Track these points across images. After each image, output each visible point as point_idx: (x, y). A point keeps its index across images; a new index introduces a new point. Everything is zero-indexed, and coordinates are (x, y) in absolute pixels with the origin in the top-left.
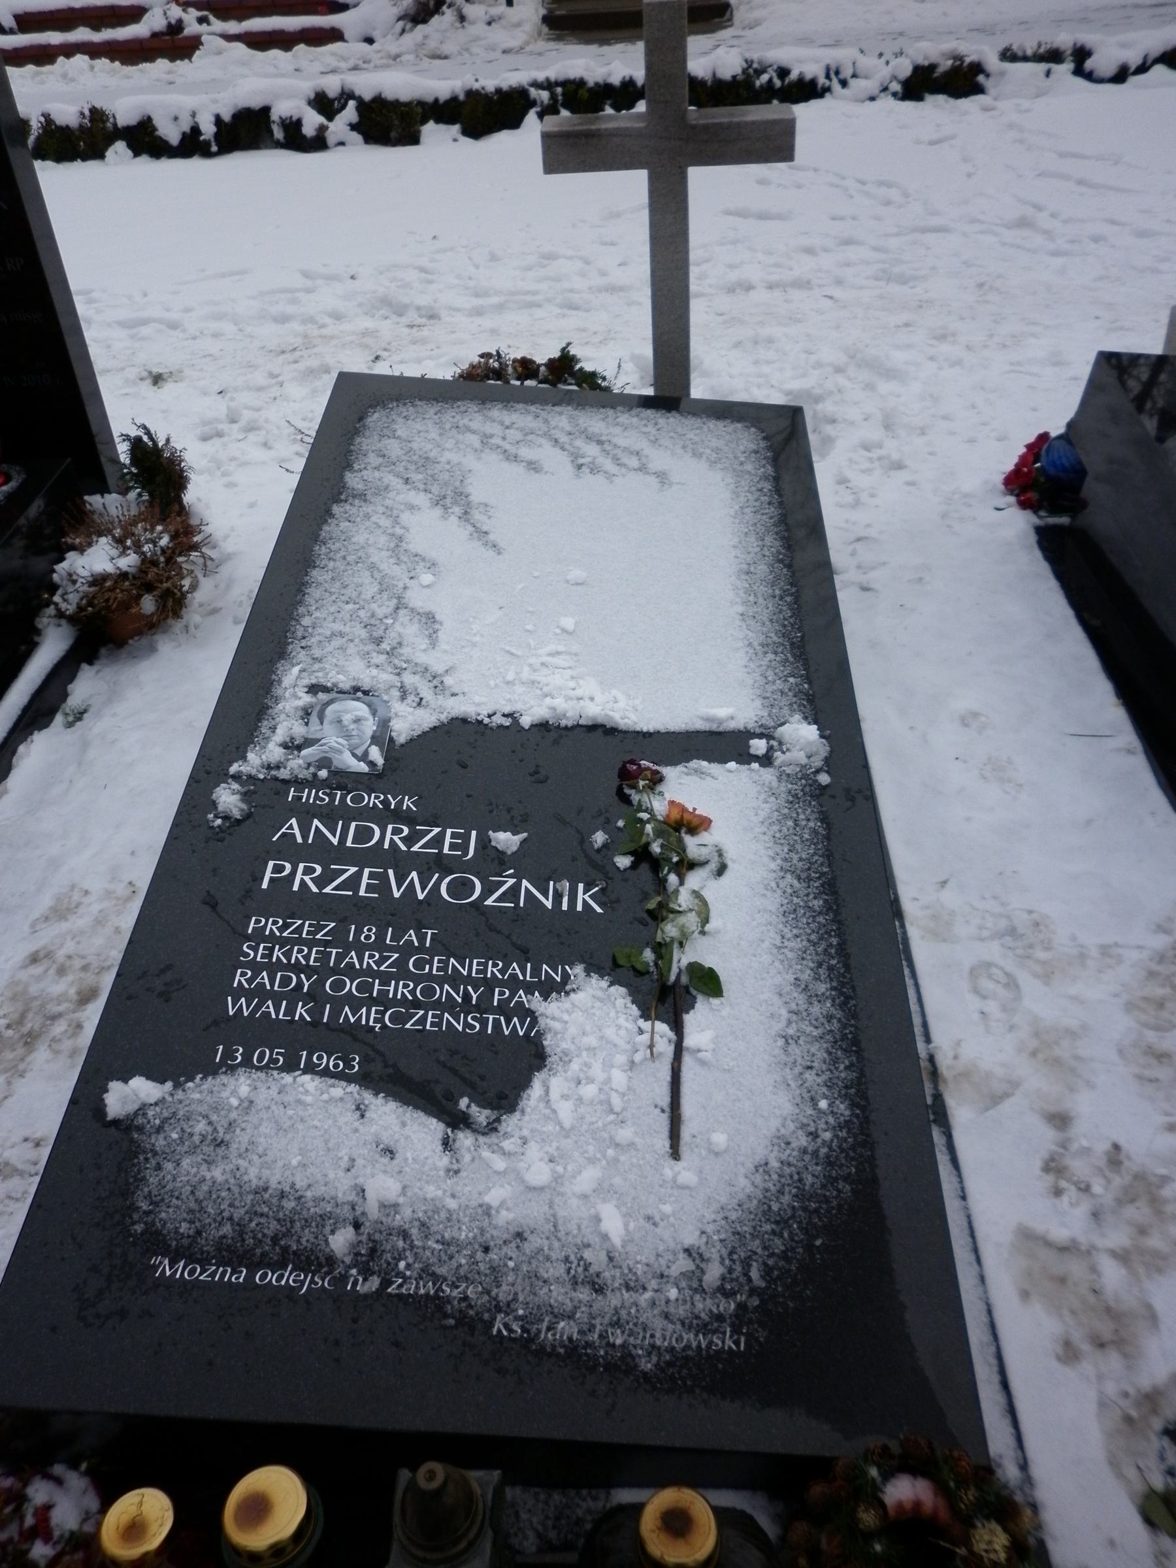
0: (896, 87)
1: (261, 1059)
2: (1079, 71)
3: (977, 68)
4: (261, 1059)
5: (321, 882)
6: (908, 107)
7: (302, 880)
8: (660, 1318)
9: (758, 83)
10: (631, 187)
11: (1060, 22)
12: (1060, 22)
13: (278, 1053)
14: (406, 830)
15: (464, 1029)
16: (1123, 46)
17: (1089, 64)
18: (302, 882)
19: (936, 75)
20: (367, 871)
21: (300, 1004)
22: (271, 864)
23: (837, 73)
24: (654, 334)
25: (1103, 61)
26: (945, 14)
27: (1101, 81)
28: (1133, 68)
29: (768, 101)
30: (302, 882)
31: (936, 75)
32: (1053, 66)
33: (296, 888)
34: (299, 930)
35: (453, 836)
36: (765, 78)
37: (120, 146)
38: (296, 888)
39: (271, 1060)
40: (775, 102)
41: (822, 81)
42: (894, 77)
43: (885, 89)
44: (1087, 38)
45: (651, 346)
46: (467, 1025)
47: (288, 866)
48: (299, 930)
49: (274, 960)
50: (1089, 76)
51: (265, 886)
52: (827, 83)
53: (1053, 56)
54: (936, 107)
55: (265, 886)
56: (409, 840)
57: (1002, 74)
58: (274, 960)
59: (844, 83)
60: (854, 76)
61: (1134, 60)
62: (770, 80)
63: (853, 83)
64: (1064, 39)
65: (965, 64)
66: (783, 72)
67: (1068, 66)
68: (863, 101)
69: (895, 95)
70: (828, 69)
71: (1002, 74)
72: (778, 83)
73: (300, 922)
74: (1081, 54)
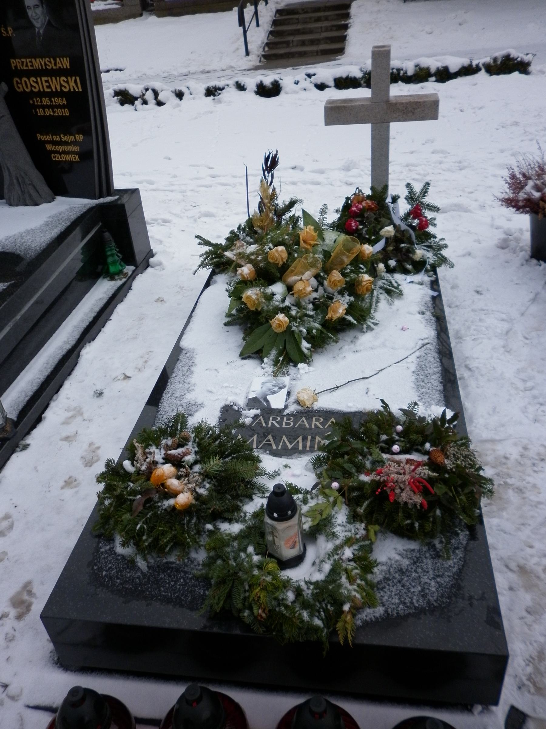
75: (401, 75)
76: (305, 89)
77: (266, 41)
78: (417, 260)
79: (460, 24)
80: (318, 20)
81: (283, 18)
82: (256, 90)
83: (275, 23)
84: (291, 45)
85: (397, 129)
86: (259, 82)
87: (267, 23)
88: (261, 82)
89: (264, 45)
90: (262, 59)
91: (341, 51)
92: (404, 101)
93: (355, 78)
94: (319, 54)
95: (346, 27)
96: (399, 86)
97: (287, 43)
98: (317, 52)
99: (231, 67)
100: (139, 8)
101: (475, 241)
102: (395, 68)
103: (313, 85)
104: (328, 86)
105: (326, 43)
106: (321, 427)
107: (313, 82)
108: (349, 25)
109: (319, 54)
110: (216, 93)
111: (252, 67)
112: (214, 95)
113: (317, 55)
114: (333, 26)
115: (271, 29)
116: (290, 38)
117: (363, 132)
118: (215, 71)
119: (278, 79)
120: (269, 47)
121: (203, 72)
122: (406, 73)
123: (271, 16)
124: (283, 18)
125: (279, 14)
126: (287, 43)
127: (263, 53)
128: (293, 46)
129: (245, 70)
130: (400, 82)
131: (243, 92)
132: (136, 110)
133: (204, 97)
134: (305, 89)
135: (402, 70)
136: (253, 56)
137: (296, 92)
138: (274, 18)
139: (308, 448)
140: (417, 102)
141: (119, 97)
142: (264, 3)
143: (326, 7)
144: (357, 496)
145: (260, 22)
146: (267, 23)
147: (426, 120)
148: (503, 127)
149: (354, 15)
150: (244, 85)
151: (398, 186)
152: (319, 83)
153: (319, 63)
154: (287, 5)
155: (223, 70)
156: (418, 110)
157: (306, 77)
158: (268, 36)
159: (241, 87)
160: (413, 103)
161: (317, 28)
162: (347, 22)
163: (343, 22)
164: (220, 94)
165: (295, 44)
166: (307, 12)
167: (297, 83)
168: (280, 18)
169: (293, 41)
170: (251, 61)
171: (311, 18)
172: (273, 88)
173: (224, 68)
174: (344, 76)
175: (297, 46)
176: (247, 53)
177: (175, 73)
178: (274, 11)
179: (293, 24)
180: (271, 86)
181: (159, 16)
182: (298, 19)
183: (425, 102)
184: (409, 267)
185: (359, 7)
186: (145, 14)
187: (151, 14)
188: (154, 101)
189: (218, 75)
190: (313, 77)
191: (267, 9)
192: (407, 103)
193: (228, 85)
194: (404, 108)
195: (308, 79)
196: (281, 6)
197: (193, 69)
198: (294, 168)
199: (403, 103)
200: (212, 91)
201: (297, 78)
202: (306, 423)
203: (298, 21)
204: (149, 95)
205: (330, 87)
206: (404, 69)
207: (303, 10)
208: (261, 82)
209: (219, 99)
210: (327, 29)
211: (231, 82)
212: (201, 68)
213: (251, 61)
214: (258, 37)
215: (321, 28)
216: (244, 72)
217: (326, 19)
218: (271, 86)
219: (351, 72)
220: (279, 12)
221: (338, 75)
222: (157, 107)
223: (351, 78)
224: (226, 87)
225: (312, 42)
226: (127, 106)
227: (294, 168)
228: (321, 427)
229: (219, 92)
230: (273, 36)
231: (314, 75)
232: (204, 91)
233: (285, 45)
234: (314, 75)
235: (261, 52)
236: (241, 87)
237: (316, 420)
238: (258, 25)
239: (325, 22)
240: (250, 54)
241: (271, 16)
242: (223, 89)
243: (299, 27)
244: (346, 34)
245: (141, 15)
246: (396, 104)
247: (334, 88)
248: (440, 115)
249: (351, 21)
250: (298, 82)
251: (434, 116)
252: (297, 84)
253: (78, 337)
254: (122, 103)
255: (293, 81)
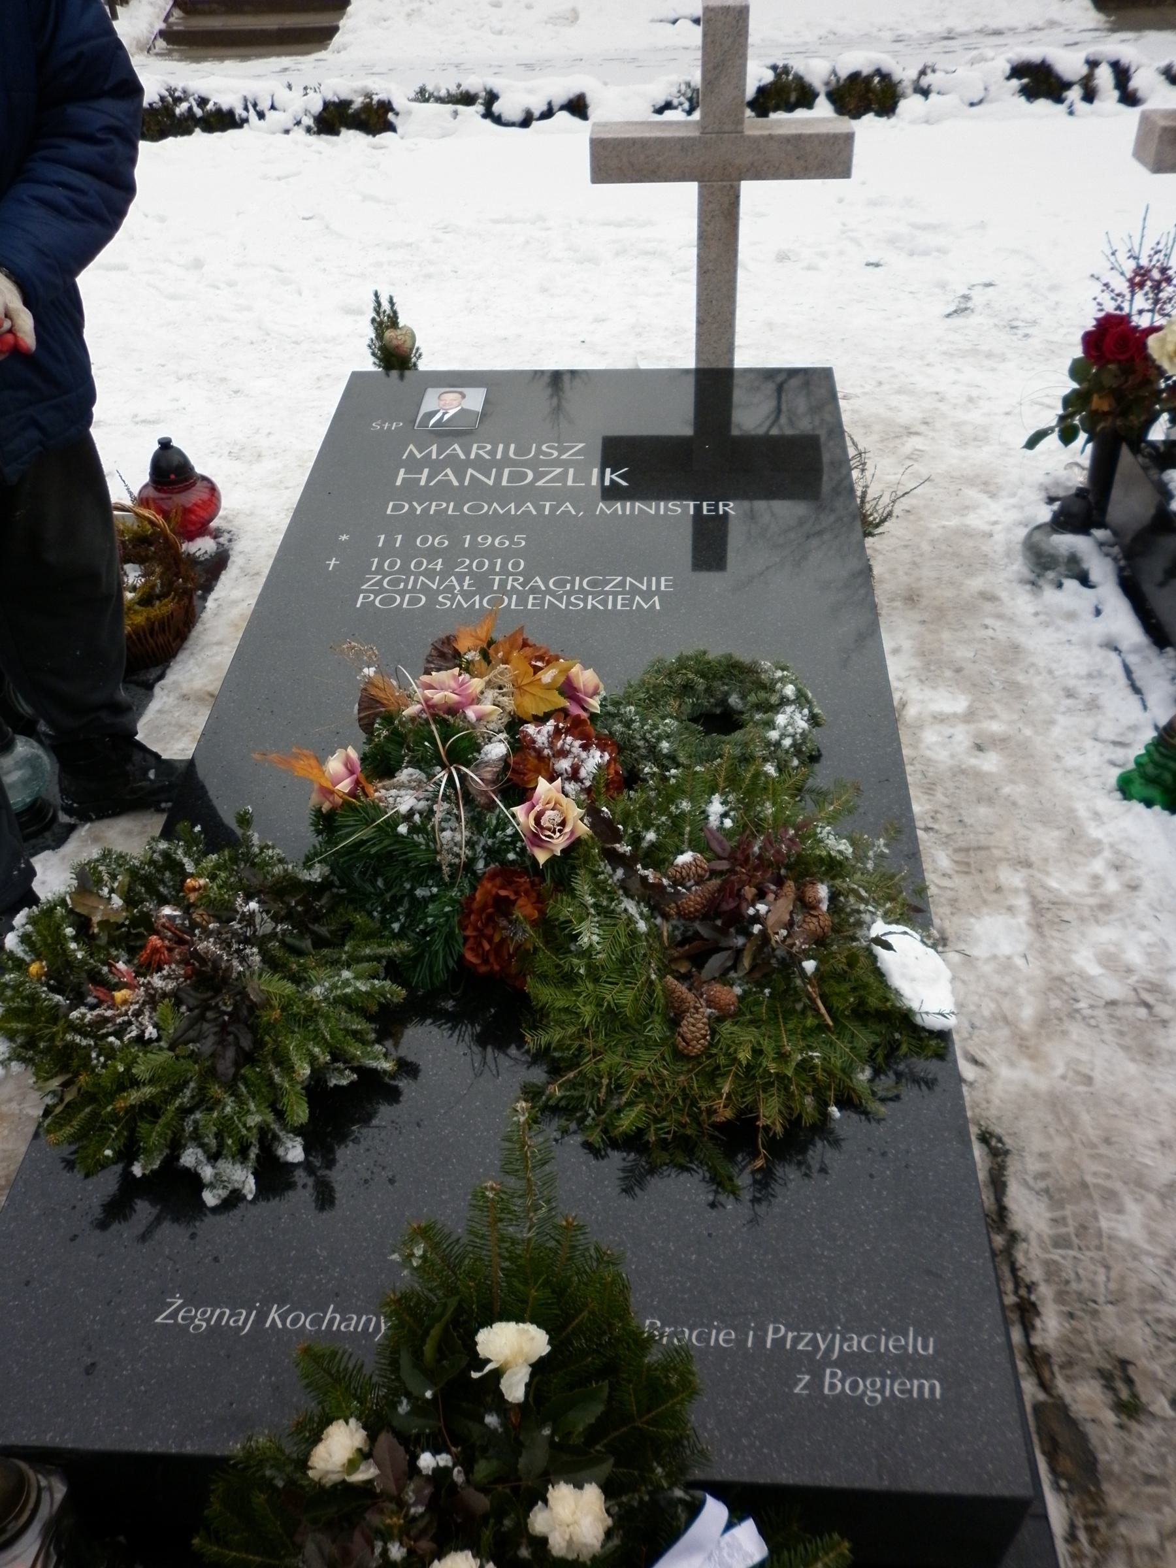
0: (308, 121)
2: (488, 114)
3: (386, 107)
6: (324, 142)
8: (553, 1556)
9: (178, 111)
11: (867, 39)
12: (867, 39)
16: (530, 91)
17: (497, 108)
19: (351, 111)
23: (255, 105)
24: (735, 271)
25: (505, 107)
26: (516, 47)
27: (512, 124)
28: (537, 114)
29: (188, 132)
31: (351, 111)
32: (460, 108)
36: (184, 106)
40: (198, 130)
41: (239, 111)
42: (306, 112)
43: (298, 123)
44: (496, 84)
45: (695, 288)
50: (498, 120)
52: (244, 114)
53: (467, 99)
54: (351, 139)
57: (409, 113)
59: (261, 115)
60: (273, 107)
61: (538, 108)
62: (190, 108)
63: (270, 115)
64: (473, 83)
65: (374, 102)
66: (203, 102)
67: (479, 108)
68: (274, 133)
69: (309, 130)
70: (245, 100)
71: (409, 113)
72: (198, 112)
74: (492, 97)
85: (754, 195)
117: (676, 204)
132: (1071, 113)
139: (611, 597)
141: (1025, 81)
144: (147, 668)
173: (1040, 24)
188: (1116, 94)
202: (540, 583)
204: (1104, 77)
212: (978, 23)
222: (1122, 108)
226: (1043, 105)
237: (514, 580)
248: (855, 170)
251: (844, 172)
254: (1030, 93)
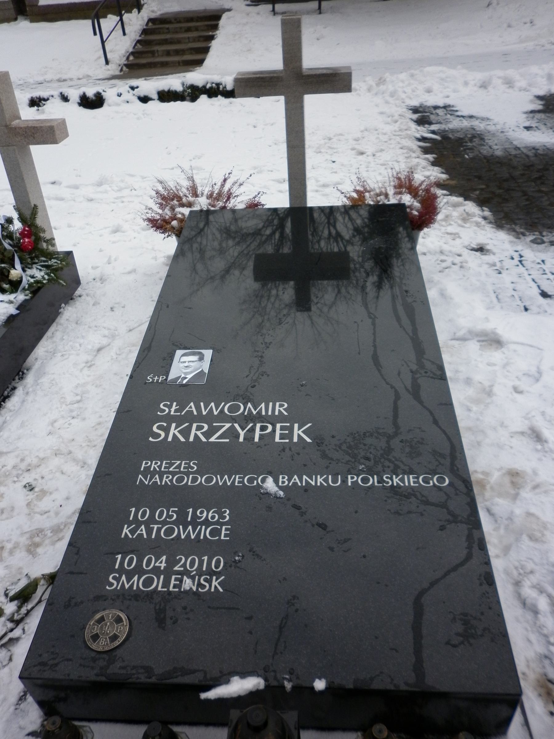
1: (160, 516)
4: (160, 516)
5: (208, 435)
7: (196, 434)
10: (314, 200)
13: (173, 511)
14: (206, 427)
15: (197, 589)
18: (196, 435)
20: (183, 462)
21: (126, 526)
22: (144, 462)
30: (196, 435)
33: (152, 469)
34: (179, 466)
35: (282, 428)
37: (159, 65)
38: (152, 469)
39: (169, 516)
46: (200, 585)
47: (150, 462)
48: (179, 466)
49: (295, 439)
51: (142, 469)
55: (142, 469)
56: (208, 435)
58: (295, 439)
73: (179, 462)
75: (221, 89)
76: (128, 102)
77: (131, 50)
78: (14, 280)
79: (318, 39)
80: (188, 30)
81: (157, 26)
82: (79, 101)
83: (145, 32)
84: (156, 55)
86: (82, 93)
87: (135, 32)
88: (84, 94)
89: (128, 54)
90: (124, 68)
91: (200, 63)
92: (22, 126)
93: (176, 92)
94: (181, 64)
95: (212, 38)
96: (219, 100)
97: (153, 53)
98: (179, 62)
99: (88, 76)
100: (12, 12)
101: (153, 258)
102: (215, 82)
103: (136, 98)
104: (151, 99)
105: (191, 54)
106: (204, 440)
107: (136, 94)
108: (215, 36)
109: (181, 64)
110: (41, 104)
111: (108, 77)
112: (38, 106)
113: (179, 65)
114: (200, 37)
115: (140, 38)
116: (156, 48)
118: (71, 79)
119: (101, 91)
120: (134, 56)
121: (59, 80)
122: (225, 87)
123: (141, 25)
124: (157, 26)
125: (152, 23)
126: (153, 53)
127: (126, 62)
128: (158, 56)
129: (99, 79)
130: (219, 96)
131: (67, 103)
133: (28, 107)
134: (128, 102)
135: (222, 84)
136: (113, 65)
137: (118, 105)
138: (145, 27)
140: (34, 127)
142: (137, 12)
143: (198, 17)
145: (126, 32)
146: (135, 32)
147: (47, 144)
148: (276, 144)
149: (223, 27)
150: (67, 96)
151: (133, 202)
152: (142, 95)
153: (172, 74)
154: (162, 15)
155: (79, 79)
156: (38, 134)
157: (130, 89)
158: (136, 45)
159: (65, 99)
160: (31, 127)
161: (185, 38)
162: (214, 33)
163: (211, 33)
164: (44, 104)
165: (160, 53)
166: (180, 22)
167: (120, 95)
168: (154, 27)
169: (158, 51)
170: (109, 70)
171: (181, 28)
172: (96, 100)
173: (81, 77)
174: (166, 89)
175: (162, 56)
176: (107, 62)
177: (31, 81)
178: (146, 20)
179: (163, 33)
180: (94, 98)
181: (32, 21)
182: (168, 29)
183: (41, 127)
184: (6, 286)
185: (229, 18)
186: (19, 17)
187: (26, 19)
189: (71, 83)
190: (136, 90)
191: (137, 18)
192: (25, 128)
193: (52, 96)
194: (24, 133)
195: (131, 91)
196: (153, 16)
197: (48, 77)
198: (53, 183)
199: (21, 128)
200: (36, 101)
201: (120, 90)
203: (168, 31)
205: (154, 100)
206: (223, 84)
207: (176, 19)
208: (84, 94)
209: (43, 110)
210: (195, 40)
211: (56, 93)
212: (58, 77)
213: (109, 70)
214: (121, 46)
215: (189, 38)
216: (98, 82)
217: (197, 29)
218: (94, 98)
219: (172, 85)
220: (151, 20)
221: (161, 89)
223: (172, 91)
224: (50, 98)
225: (177, 52)
227: (53, 183)
228: (204, 440)
229: (44, 102)
230: (140, 44)
231: (137, 87)
232: (28, 102)
233: (150, 55)
234: (137, 87)
235: (124, 61)
236: (65, 99)
238: (124, 34)
239: (195, 32)
240: (110, 63)
241: (141, 25)
242: (48, 99)
243: (168, 36)
244: (210, 45)
245: (16, 19)
246: (15, 128)
247: (158, 101)
249: (218, 32)
250: (121, 94)
252: (120, 96)
253: (41, 350)
255: (116, 93)
